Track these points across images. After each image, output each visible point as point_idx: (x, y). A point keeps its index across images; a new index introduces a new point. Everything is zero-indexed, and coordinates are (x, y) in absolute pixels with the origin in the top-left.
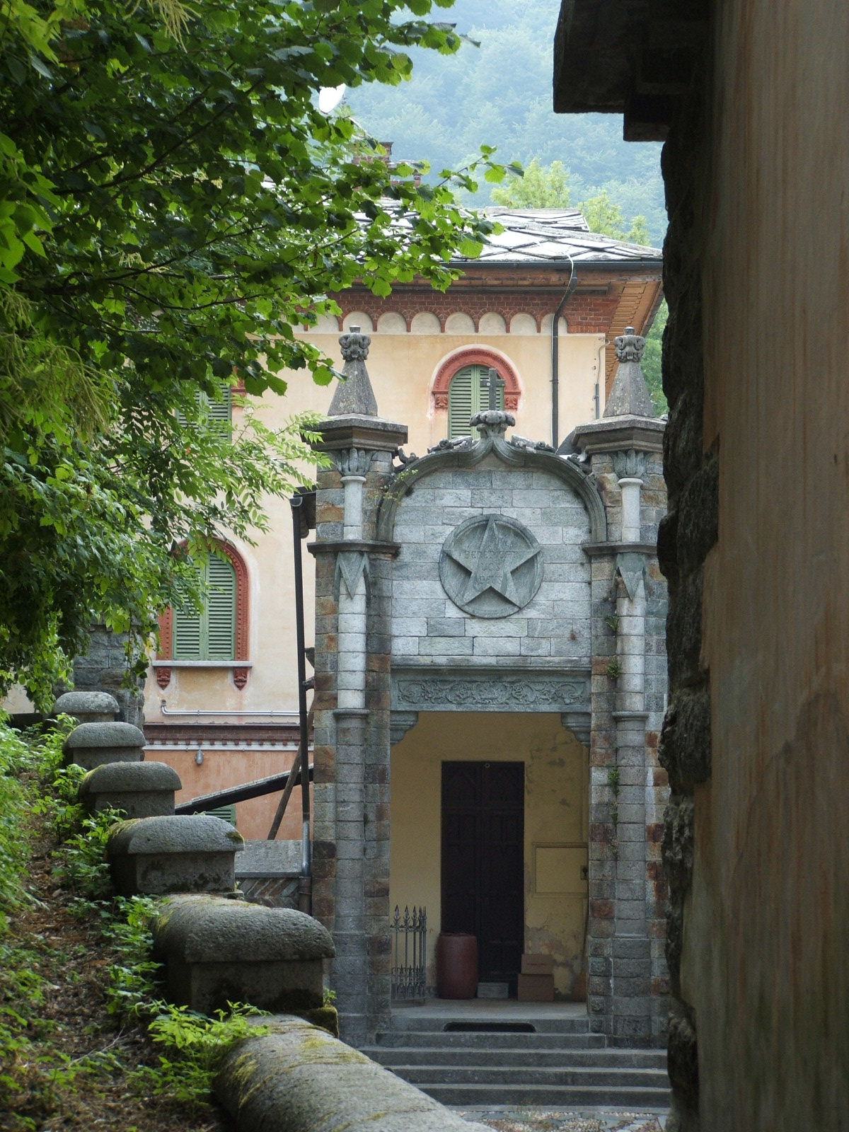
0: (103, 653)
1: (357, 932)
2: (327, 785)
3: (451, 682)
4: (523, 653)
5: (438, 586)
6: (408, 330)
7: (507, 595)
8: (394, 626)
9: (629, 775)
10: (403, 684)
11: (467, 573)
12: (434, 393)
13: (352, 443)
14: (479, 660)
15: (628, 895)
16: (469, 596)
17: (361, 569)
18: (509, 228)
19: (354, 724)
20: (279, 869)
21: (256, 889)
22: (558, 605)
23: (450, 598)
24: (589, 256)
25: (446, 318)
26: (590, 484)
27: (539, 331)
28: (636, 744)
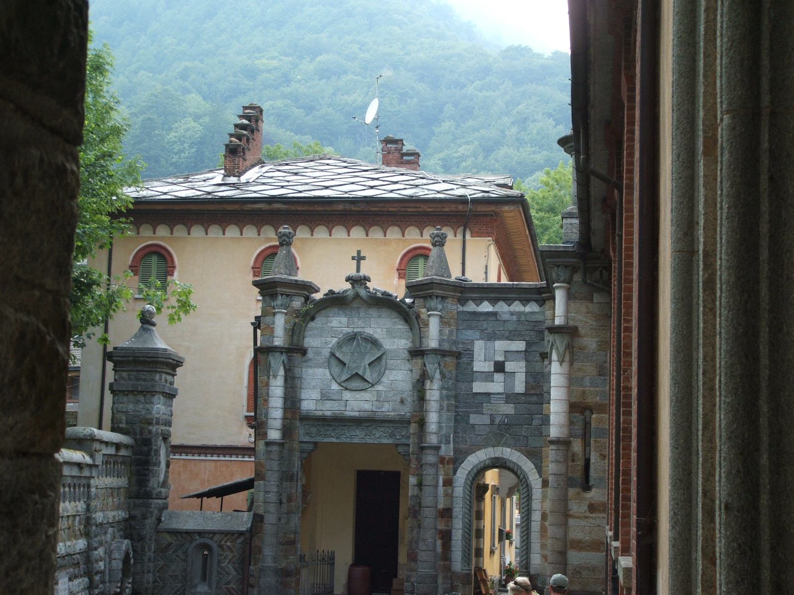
0: (141, 406)
1: (273, 565)
2: (261, 482)
3: (332, 426)
4: (374, 410)
5: (327, 371)
6: (385, 236)
7: (365, 377)
8: (303, 394)
9: (428, 480)
10: (307, 427)
11: (344, 364)
12: (398, 270)
13: (277, 291)
14: (349, 414)
15: (424, 548)
16: (344, 377)
17: (281, 361)
18: (444, 181)
19: (275, 448)
20: (236, 528)
21: (223, 539)
22: (394, 383)
23: (334, 378)
24: (480, 195)
25: (405, 229)
26: (412, 315)
27: (455, 236)
28: (432, 462)
